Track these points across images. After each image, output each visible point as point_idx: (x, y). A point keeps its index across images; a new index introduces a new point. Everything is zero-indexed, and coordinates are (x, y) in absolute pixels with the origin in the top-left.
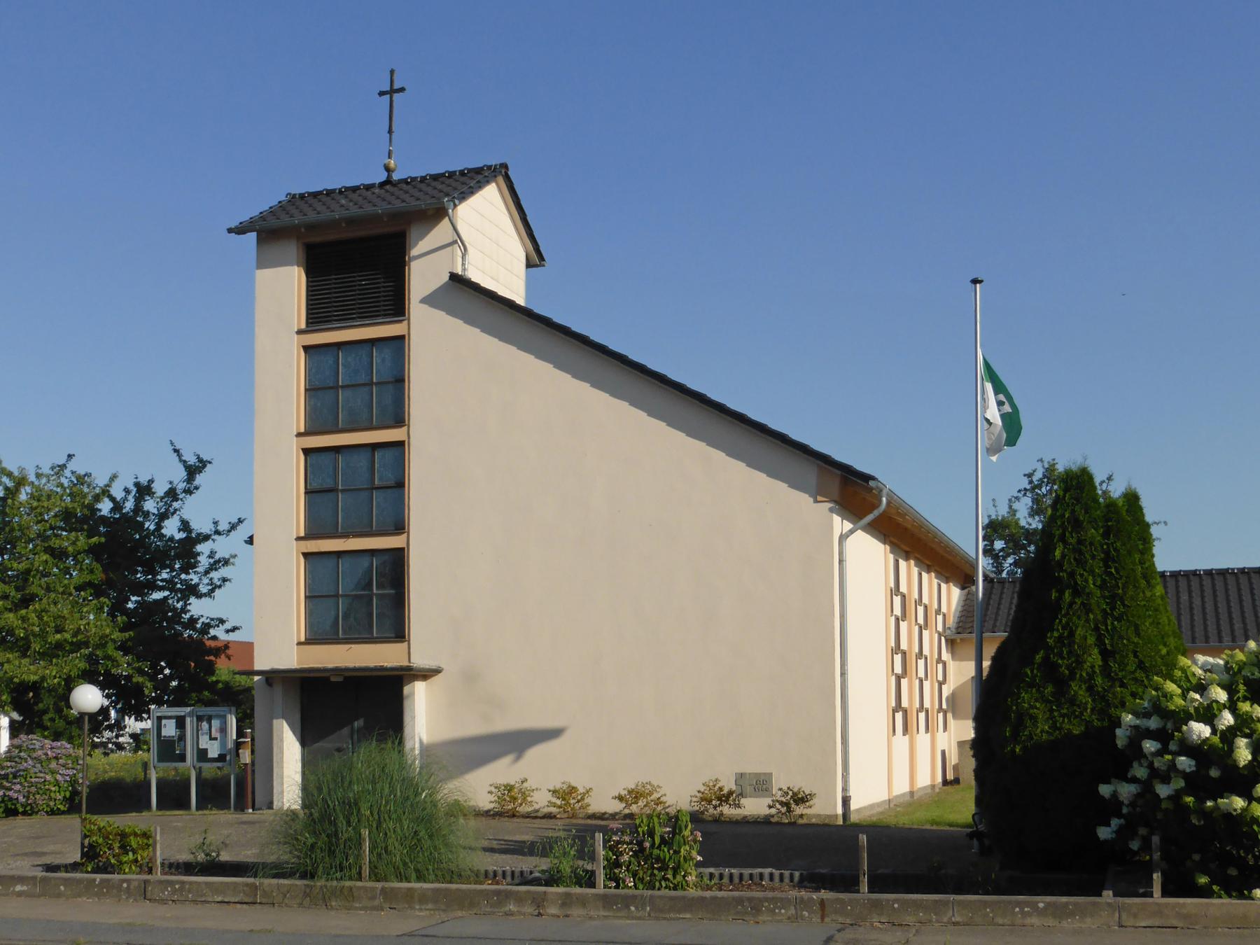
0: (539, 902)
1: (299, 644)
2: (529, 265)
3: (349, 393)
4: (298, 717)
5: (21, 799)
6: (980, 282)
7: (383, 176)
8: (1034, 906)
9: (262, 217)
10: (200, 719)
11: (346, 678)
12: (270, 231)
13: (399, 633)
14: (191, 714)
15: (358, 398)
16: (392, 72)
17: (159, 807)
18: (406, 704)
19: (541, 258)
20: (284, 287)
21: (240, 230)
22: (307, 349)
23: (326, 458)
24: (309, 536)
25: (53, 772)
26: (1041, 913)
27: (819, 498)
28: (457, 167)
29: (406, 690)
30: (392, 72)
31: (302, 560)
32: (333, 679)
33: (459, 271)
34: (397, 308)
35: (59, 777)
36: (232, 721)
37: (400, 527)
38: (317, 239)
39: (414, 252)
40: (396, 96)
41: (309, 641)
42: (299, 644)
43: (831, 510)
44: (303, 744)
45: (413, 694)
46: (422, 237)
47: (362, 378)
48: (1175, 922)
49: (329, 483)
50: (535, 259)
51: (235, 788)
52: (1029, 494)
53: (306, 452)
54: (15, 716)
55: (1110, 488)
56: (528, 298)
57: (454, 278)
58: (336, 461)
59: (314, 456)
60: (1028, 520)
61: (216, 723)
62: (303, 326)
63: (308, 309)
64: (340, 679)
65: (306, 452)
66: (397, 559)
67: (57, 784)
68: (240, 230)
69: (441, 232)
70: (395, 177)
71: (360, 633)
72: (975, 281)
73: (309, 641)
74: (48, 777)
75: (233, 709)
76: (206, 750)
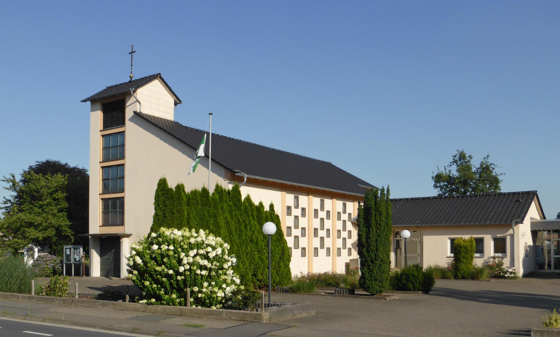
0: (18, 297)
2: (176, 104)
3: (113, 149)
4: (99, 248)
6: (212, 114)
8: (99, 302)
9: (91, 97)
10: (75, 249)
11: (107, 237)
13: (122, 224)
15: (114, 149)
17: (75, 275)
19: (180, 101)
21: (85, 101)
23: (106, 169)
25: (47, 265)
29: (121, 240)
31: (101, 201)
33: (138, 111)
36: (82, 250)
37: (122, 190)
39: (127, 105)
40: (133, 54)
41: (103, 226)
43: (229, 183)
46: (129, 100)
47: (116, 145)
49: (107, 178)
50: (178, 101)
51: (83, 270)
55: (488, 160)
56: (175, 115)
57: (135, 113)
58: (109, 171)
62: (102, 129)
66: (122, 199)
67: (48, 268)
68: (85, 101)
69: (132, 100)
70: (133, 79)
72: (210, 114)
73: (103, 226)
76: (182, 259)
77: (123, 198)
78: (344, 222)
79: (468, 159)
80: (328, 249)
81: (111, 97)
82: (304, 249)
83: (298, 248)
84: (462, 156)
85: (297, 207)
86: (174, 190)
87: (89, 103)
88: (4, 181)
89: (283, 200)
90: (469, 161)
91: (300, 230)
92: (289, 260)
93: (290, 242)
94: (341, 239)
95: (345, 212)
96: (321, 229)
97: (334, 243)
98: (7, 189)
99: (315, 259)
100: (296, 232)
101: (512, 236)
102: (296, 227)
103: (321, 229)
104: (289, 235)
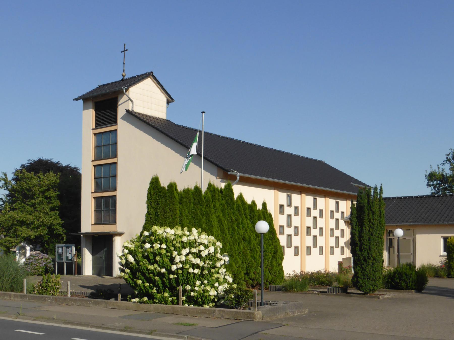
0: (10, 296)
1: (92, 225)
2: (168, 102)
4: (91, 247)
5: (30, 271)
6: (204, 113)
7: (121, 78)
8: (91, 301)
9: (83, 95)
10: (67, 247)
12: (87, 99)
14: (64, 246)
15: (106, 148)
16: (125, 45)
18: (113, 243)
19: (172, 99)
20: (90, 115)
21: (77, 99)
22: (95, 134)
24: (95, 192)
25: (39, 263)
26: (93, 303)
27: (218, 178)
28: (139, 74)
29: (113, 239)
30: (125, 45)
32: (95, 236)
33: (130, 109)
34: (115, 122)
35: (41, 265)
36: (74, 248)
38: (98, 100)
39: (119, 103)
41: (95, 224)
42: (92, 225)
43: (221, 182)
44: (93, 255)
45: (115, 240)
48: (116, 308)
49: (100, 176)
50: (170, 100)
52: (448, 162)
53: (95, 166)
54: (31, 246)
56: (168, 112)
57: (127, 111)
58: (101, 169)
59: (96, 167)
60: (447, 170)
61: (70, 248)
62: (94, 127)
63: (96, 122)
64: (97, 236)
65: (95, 166)
66: (114, 198)
67: (40, 267)
68: (77, 99)
69: (124, 98)
70: (125, 78)
71: (106, 223)
72: (202, 113)
73: (95, 224)
74: (37, 265)
75: (74, 245)
78: (337, 220)
83: (291, 247)
95: (337, 211)
97: (326, 241)
99: (331, 257)
102: (289, 225)
104: (282, 233)
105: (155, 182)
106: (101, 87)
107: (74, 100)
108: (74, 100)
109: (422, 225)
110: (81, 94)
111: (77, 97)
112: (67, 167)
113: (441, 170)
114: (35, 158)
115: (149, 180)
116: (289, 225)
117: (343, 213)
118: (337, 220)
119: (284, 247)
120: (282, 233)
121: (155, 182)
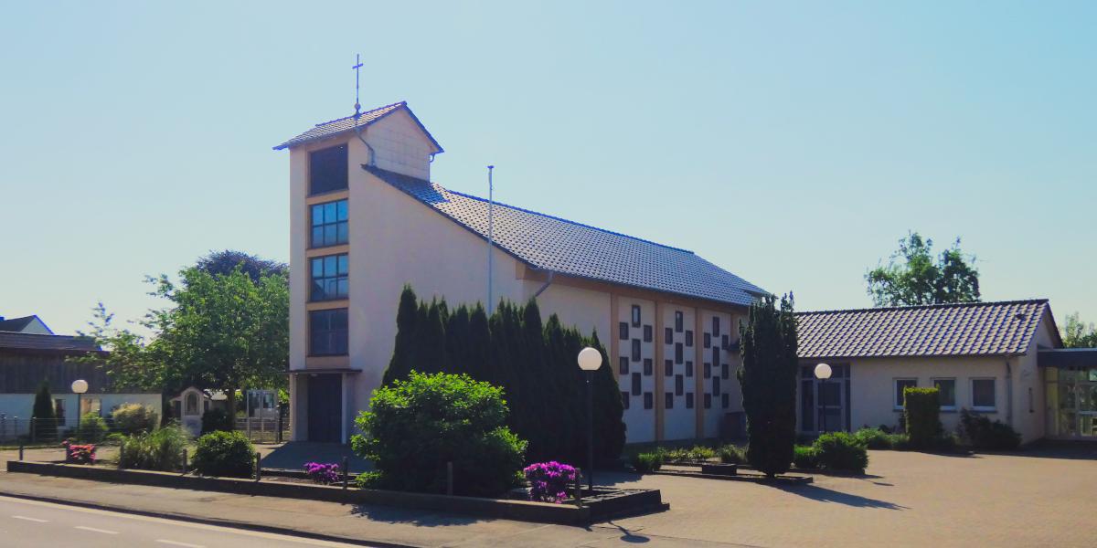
21: (280, 148)
34: (343, 184)
38: (314, 148)
68: (280, 148)
77: (346, 309)
78: (716, 350)
79: (926, 245)
80: (690, 396)
81: (319, 138)
82: (648, 395)
83: (639, 393)
84: (917, 241)
85: (637, 325)
86: (469, 317)
87: (287, 150)
88: (147, 281)
89: (614, 313)
90: (927, 250)
91: (641, 363)
92: (456, 524)
93: (624, 383)
94: (642, 396)
95: (716, 333)
96: (687, 345)
97: (698, 385)
98: (153, 294)
99: (667, 412)
100: (636, 367)
101: (848, 384)
102: (637, 357)
103: (687, 345)
104: (624, 371)
105: (408, 297)
106: (488, 522)
107: (274, 149)
108: (274, 149)
109: (112, 445)
110: (286, 140)
111: (279, 144)
112: (391, 365)
113: (892, 270)
114: (220, 249)
115: (363, 170)
116: (637, 357)
117: (725, 338)
118: (716, 350)
119: (626, 394)
120: (624, 371)
121: (408, 297)
